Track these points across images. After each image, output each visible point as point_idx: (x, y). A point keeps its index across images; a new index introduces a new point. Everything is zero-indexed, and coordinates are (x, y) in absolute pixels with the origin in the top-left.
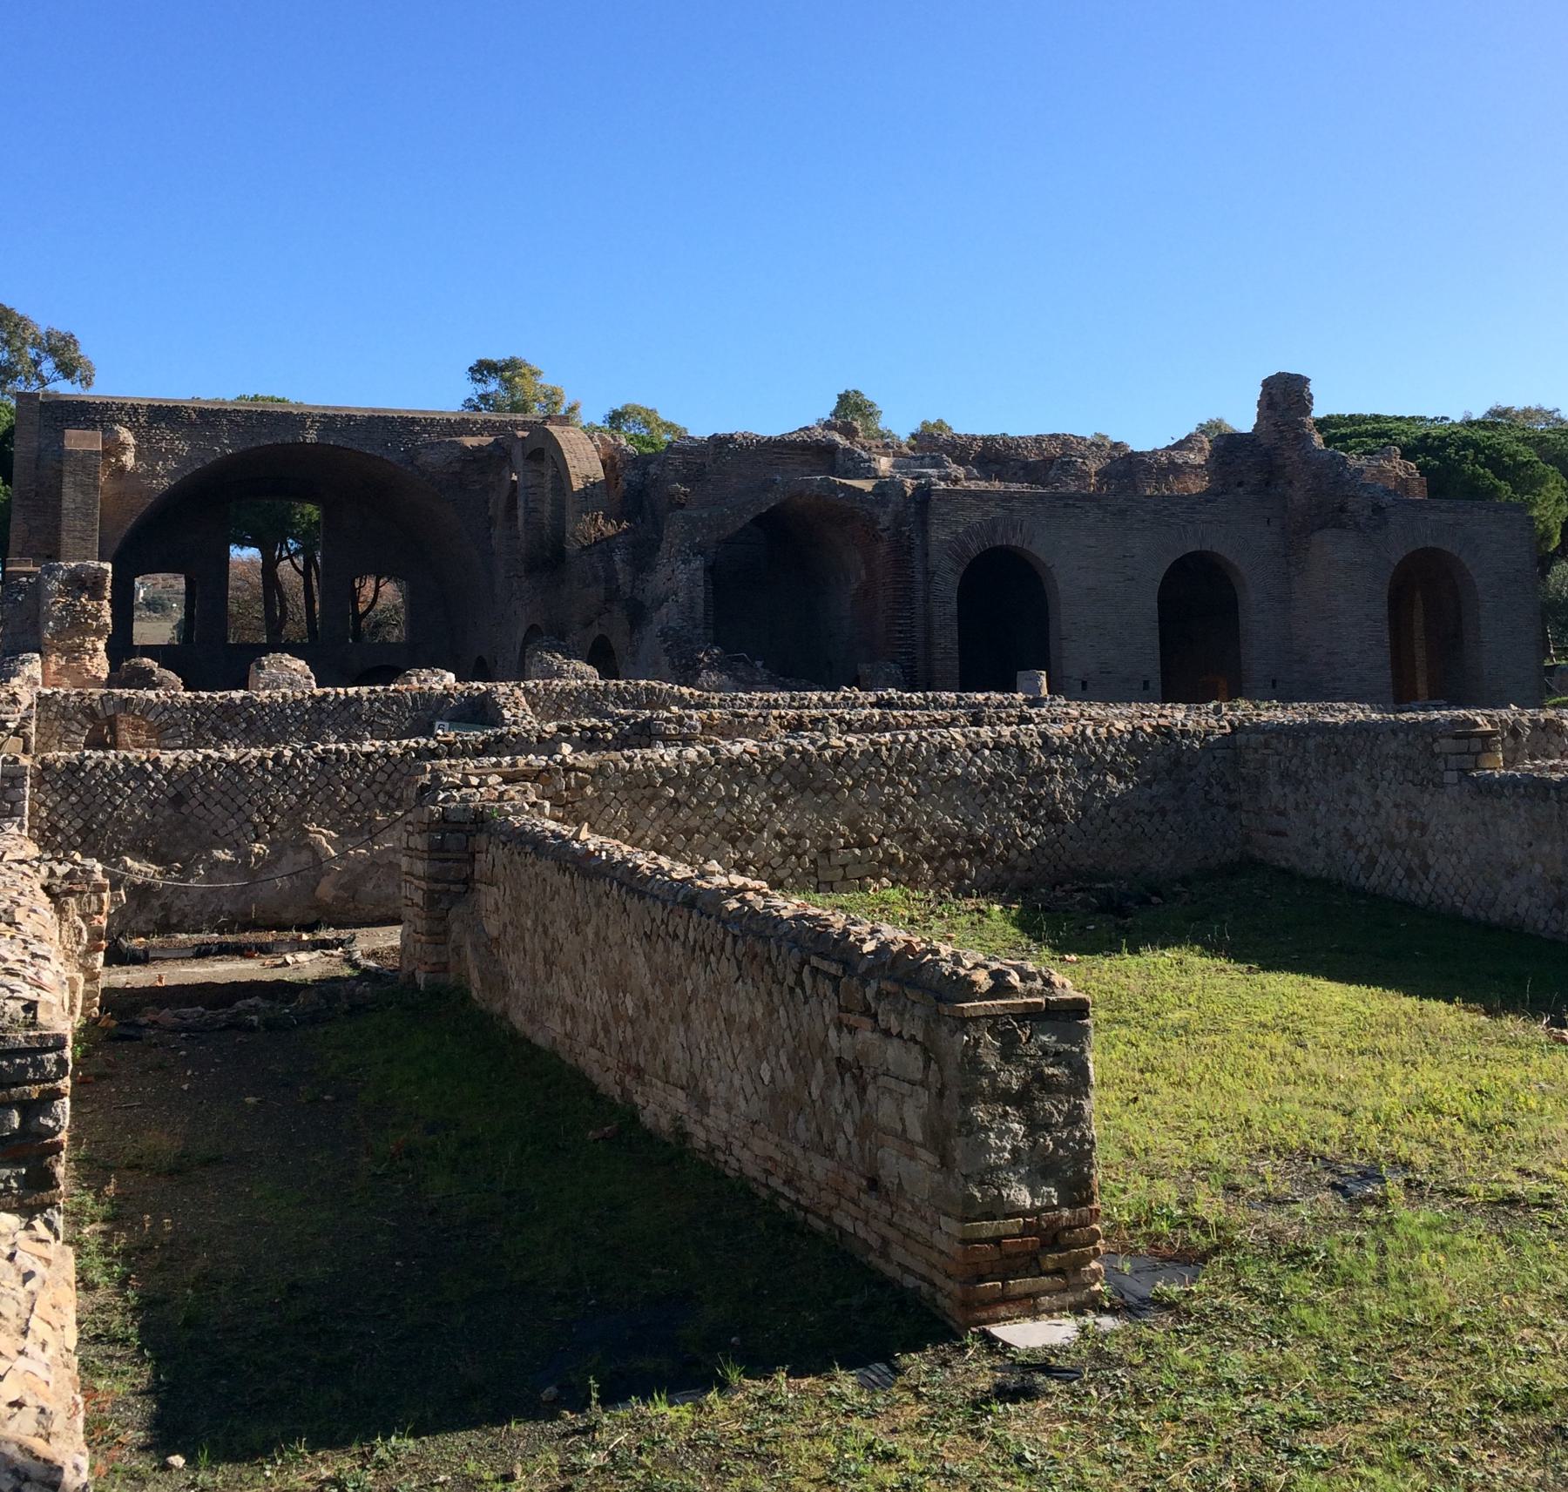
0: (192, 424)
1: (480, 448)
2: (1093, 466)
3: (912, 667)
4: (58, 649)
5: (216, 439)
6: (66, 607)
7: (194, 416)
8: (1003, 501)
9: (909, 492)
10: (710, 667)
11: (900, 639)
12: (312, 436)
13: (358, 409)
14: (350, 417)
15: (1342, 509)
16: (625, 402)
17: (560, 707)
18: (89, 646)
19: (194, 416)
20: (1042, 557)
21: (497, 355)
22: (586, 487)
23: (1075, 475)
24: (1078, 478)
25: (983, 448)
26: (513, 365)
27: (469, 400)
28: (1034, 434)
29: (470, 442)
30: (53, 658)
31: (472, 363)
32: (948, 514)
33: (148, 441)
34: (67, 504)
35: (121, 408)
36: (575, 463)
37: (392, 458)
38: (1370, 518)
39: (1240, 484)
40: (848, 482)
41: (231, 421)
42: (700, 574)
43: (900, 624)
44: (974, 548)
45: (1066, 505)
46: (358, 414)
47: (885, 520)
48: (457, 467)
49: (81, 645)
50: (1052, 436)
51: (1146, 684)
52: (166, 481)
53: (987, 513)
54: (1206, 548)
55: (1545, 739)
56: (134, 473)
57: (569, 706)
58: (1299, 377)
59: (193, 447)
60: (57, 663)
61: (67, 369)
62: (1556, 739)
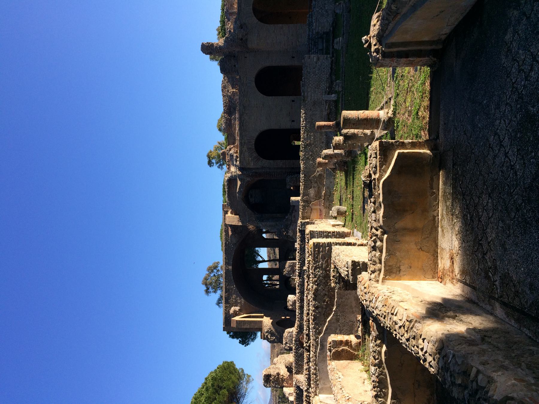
0: (229, 294)
1: (232, 231)
2: (231, 90)
3: (288, 173)
4: (282, 383)
5: (232, 289)
6: (273, 383)
7: (227, 294)
8: (242, 146)
9: (240, 173)
10: (287, 232)
11: (280, 176)
12: (230, 267)
13: (223, 256)
14: (225, 258)
15: (242, 39)
16: (217, 128)
17: (299, 364)
18: (281, 377)
19: (227, 294)
20: (257, 134)
21: (207, 160)
22: (241, 222)
23: (234, 96)
24: (234, 96)
25: (227, 114)
26: (209, 156)
27: (218, 167)
28: (222, 97)
29: (230, 233)
30: (284, 385)
31: (209, 166)
32: (246, 162)
33: (233, 304)
34: (248, 327)
35: (225, 310)
36: (235, 223)
37: (235, 248)
38: (244, 30)
39: (235, 66)
40: (238, 187)
41: (228, 286)
42: (263, 223)
43: (276, 175)
44: (255, 154)
45: (243, 126)
46: (224, 256)
47: (248, 179)
48: (236, 235)
49: (281, 379)
50: (222, 91)
51: (293, 101)
52: (242, 300)
53: (246, 150)
54: (254, 80)
55: (319, 296)
56: (241, 307)
57: (299, 362)
58: (202, 46)
59: (234, 294)
60: (285, 384)
61: (216, 267)
62: (319, 292)
